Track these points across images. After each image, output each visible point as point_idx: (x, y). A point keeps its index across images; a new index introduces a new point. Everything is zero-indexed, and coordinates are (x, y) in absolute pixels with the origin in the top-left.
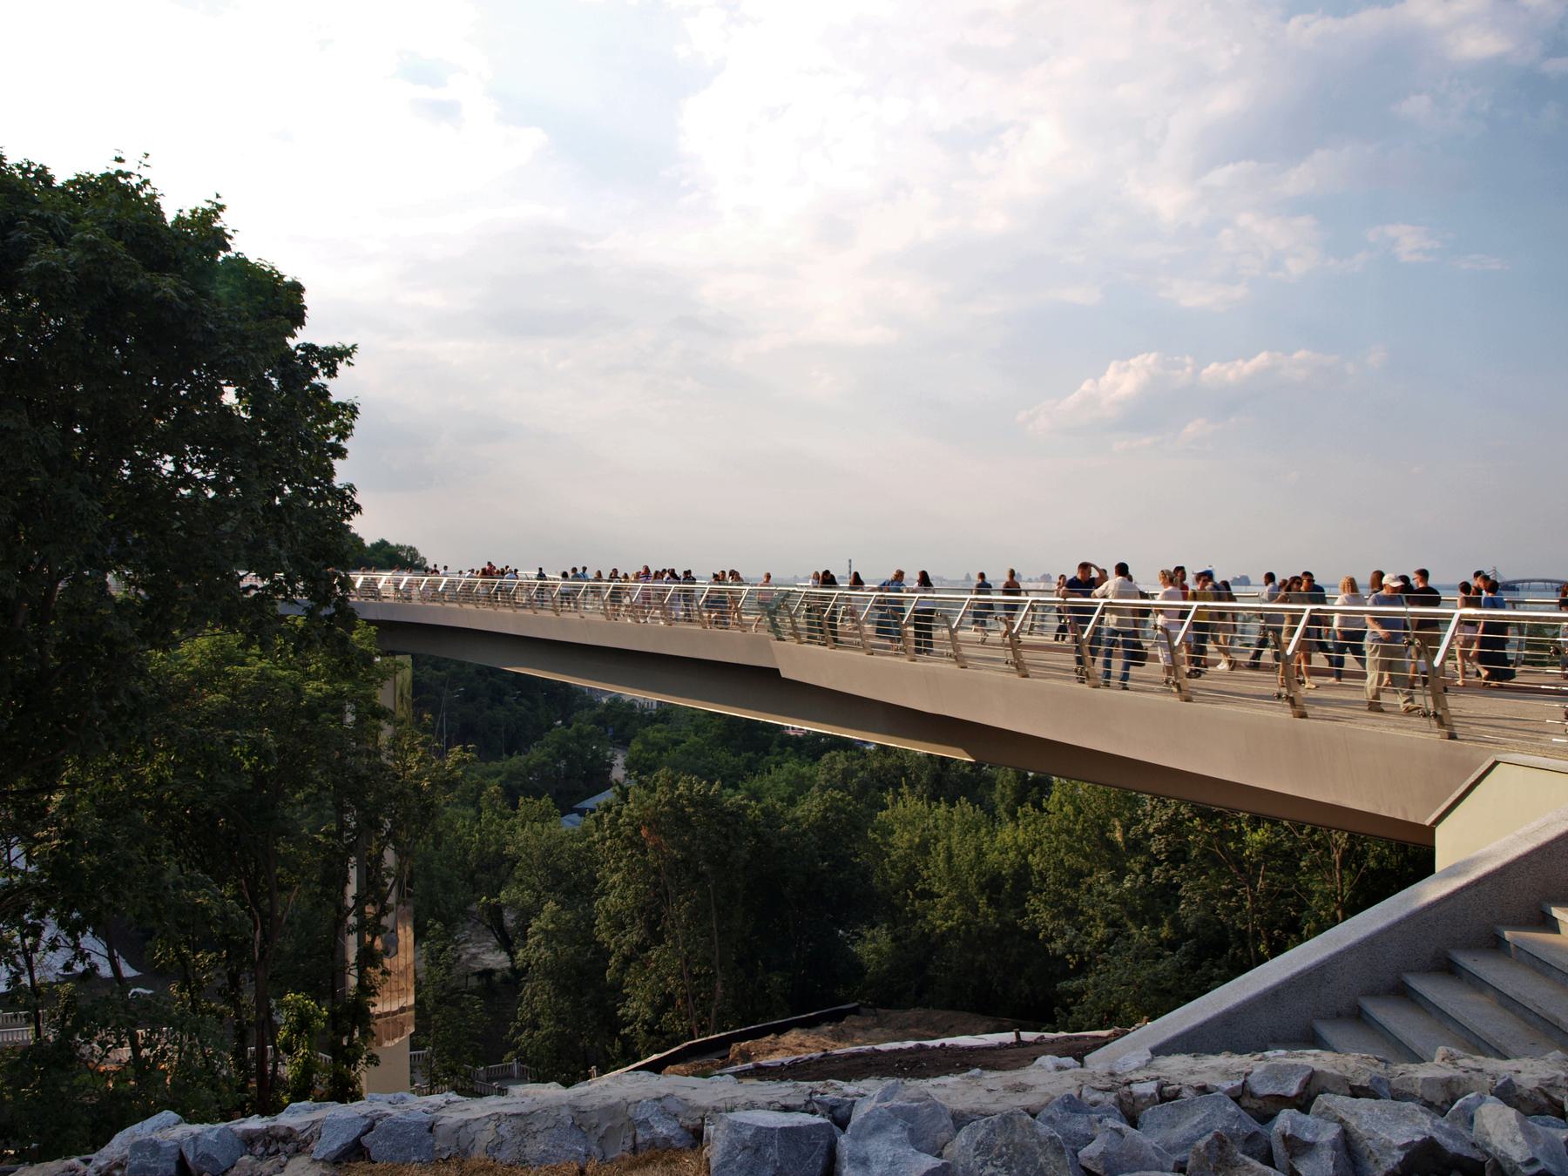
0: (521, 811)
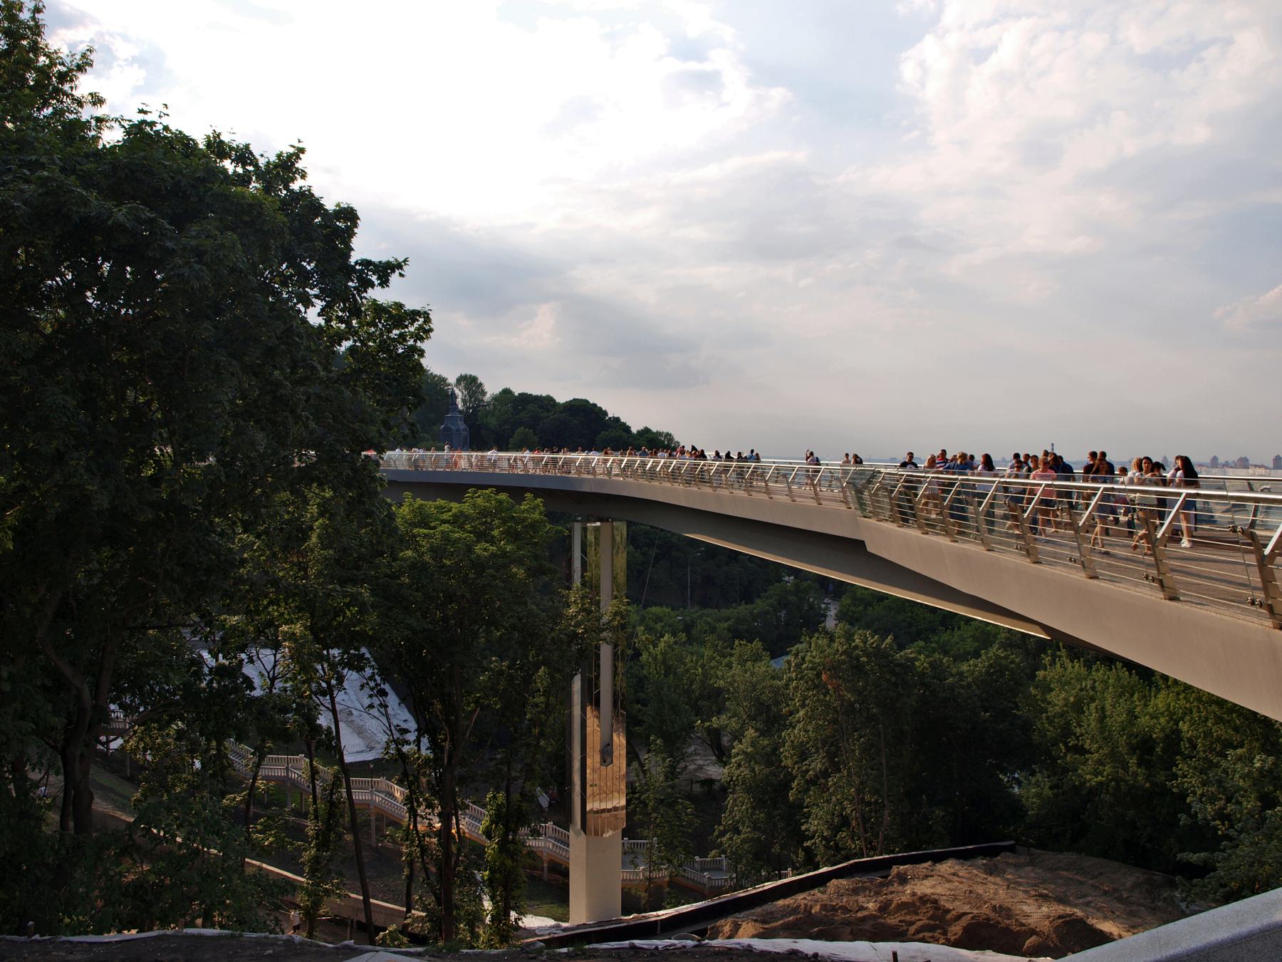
0: (737, 651)
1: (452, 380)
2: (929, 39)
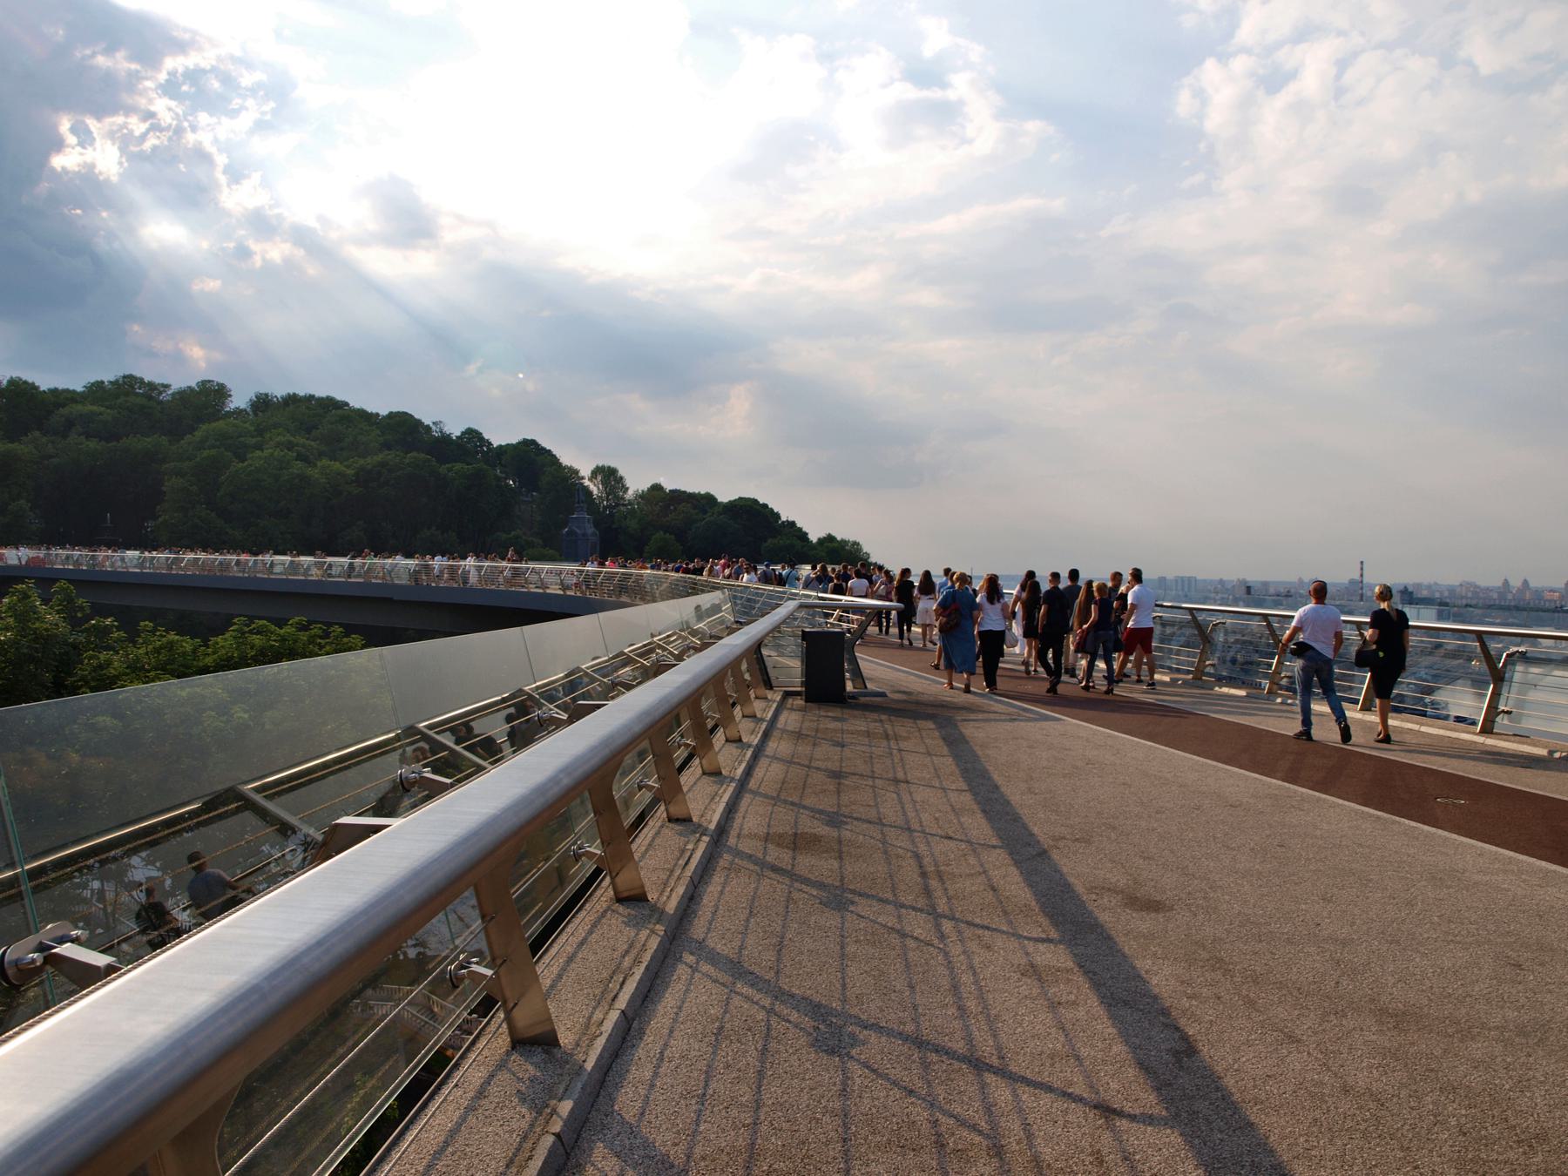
1: (585, 471)
2: (1210, 64)
